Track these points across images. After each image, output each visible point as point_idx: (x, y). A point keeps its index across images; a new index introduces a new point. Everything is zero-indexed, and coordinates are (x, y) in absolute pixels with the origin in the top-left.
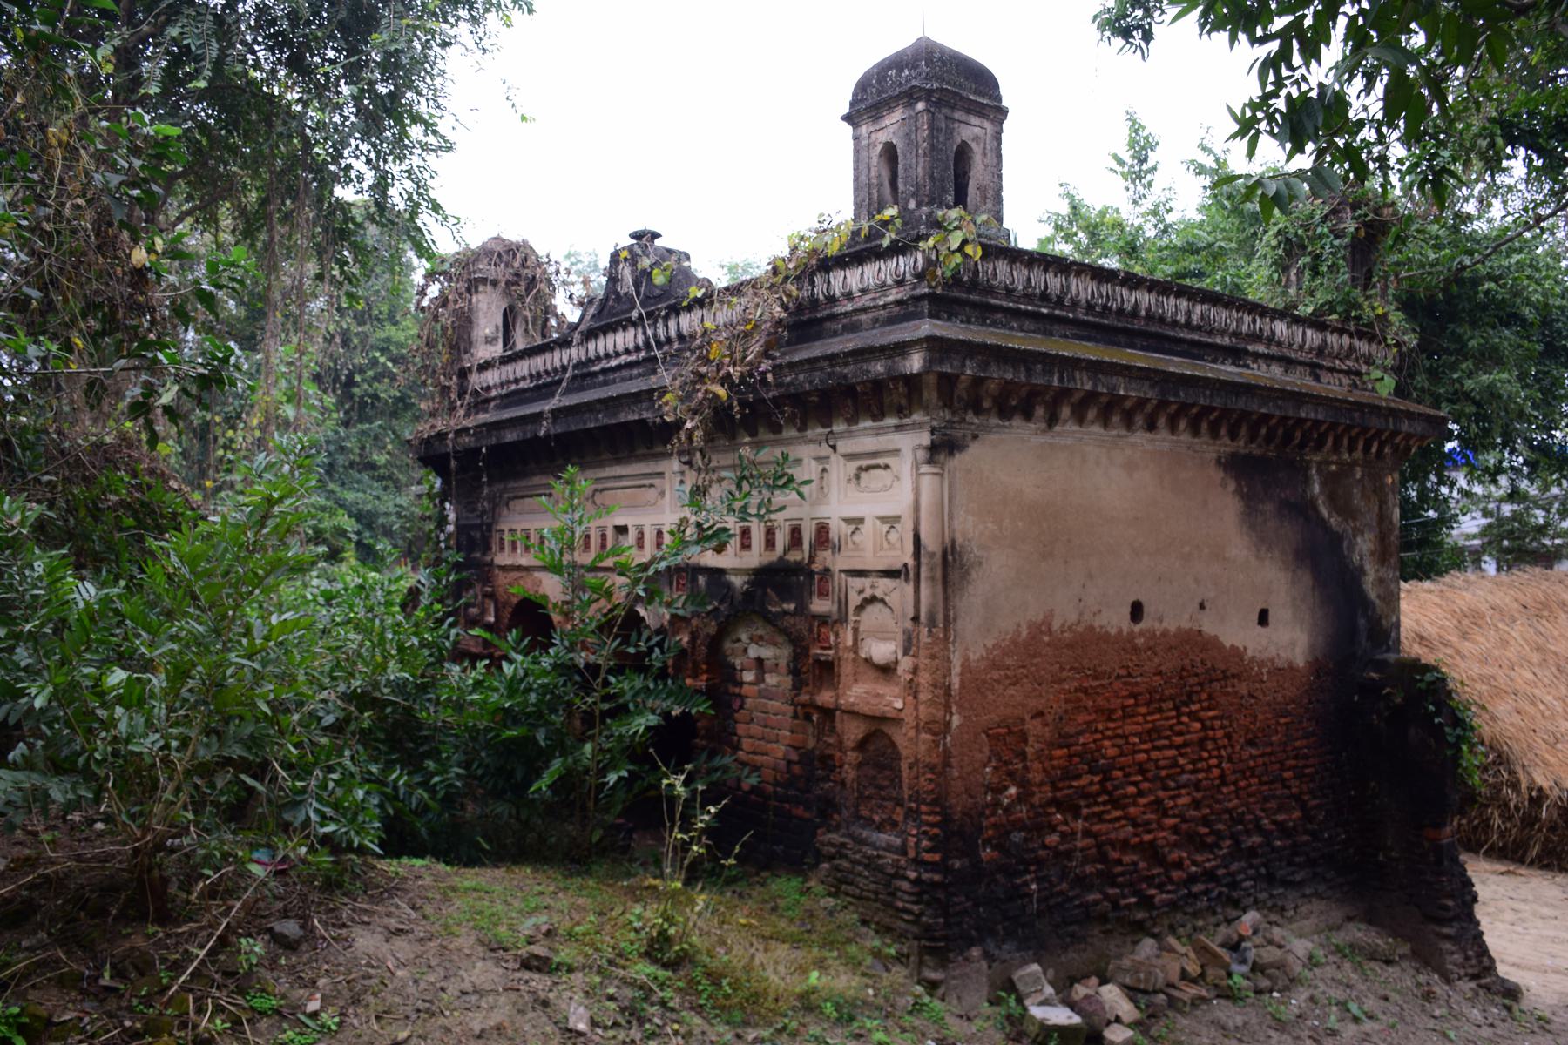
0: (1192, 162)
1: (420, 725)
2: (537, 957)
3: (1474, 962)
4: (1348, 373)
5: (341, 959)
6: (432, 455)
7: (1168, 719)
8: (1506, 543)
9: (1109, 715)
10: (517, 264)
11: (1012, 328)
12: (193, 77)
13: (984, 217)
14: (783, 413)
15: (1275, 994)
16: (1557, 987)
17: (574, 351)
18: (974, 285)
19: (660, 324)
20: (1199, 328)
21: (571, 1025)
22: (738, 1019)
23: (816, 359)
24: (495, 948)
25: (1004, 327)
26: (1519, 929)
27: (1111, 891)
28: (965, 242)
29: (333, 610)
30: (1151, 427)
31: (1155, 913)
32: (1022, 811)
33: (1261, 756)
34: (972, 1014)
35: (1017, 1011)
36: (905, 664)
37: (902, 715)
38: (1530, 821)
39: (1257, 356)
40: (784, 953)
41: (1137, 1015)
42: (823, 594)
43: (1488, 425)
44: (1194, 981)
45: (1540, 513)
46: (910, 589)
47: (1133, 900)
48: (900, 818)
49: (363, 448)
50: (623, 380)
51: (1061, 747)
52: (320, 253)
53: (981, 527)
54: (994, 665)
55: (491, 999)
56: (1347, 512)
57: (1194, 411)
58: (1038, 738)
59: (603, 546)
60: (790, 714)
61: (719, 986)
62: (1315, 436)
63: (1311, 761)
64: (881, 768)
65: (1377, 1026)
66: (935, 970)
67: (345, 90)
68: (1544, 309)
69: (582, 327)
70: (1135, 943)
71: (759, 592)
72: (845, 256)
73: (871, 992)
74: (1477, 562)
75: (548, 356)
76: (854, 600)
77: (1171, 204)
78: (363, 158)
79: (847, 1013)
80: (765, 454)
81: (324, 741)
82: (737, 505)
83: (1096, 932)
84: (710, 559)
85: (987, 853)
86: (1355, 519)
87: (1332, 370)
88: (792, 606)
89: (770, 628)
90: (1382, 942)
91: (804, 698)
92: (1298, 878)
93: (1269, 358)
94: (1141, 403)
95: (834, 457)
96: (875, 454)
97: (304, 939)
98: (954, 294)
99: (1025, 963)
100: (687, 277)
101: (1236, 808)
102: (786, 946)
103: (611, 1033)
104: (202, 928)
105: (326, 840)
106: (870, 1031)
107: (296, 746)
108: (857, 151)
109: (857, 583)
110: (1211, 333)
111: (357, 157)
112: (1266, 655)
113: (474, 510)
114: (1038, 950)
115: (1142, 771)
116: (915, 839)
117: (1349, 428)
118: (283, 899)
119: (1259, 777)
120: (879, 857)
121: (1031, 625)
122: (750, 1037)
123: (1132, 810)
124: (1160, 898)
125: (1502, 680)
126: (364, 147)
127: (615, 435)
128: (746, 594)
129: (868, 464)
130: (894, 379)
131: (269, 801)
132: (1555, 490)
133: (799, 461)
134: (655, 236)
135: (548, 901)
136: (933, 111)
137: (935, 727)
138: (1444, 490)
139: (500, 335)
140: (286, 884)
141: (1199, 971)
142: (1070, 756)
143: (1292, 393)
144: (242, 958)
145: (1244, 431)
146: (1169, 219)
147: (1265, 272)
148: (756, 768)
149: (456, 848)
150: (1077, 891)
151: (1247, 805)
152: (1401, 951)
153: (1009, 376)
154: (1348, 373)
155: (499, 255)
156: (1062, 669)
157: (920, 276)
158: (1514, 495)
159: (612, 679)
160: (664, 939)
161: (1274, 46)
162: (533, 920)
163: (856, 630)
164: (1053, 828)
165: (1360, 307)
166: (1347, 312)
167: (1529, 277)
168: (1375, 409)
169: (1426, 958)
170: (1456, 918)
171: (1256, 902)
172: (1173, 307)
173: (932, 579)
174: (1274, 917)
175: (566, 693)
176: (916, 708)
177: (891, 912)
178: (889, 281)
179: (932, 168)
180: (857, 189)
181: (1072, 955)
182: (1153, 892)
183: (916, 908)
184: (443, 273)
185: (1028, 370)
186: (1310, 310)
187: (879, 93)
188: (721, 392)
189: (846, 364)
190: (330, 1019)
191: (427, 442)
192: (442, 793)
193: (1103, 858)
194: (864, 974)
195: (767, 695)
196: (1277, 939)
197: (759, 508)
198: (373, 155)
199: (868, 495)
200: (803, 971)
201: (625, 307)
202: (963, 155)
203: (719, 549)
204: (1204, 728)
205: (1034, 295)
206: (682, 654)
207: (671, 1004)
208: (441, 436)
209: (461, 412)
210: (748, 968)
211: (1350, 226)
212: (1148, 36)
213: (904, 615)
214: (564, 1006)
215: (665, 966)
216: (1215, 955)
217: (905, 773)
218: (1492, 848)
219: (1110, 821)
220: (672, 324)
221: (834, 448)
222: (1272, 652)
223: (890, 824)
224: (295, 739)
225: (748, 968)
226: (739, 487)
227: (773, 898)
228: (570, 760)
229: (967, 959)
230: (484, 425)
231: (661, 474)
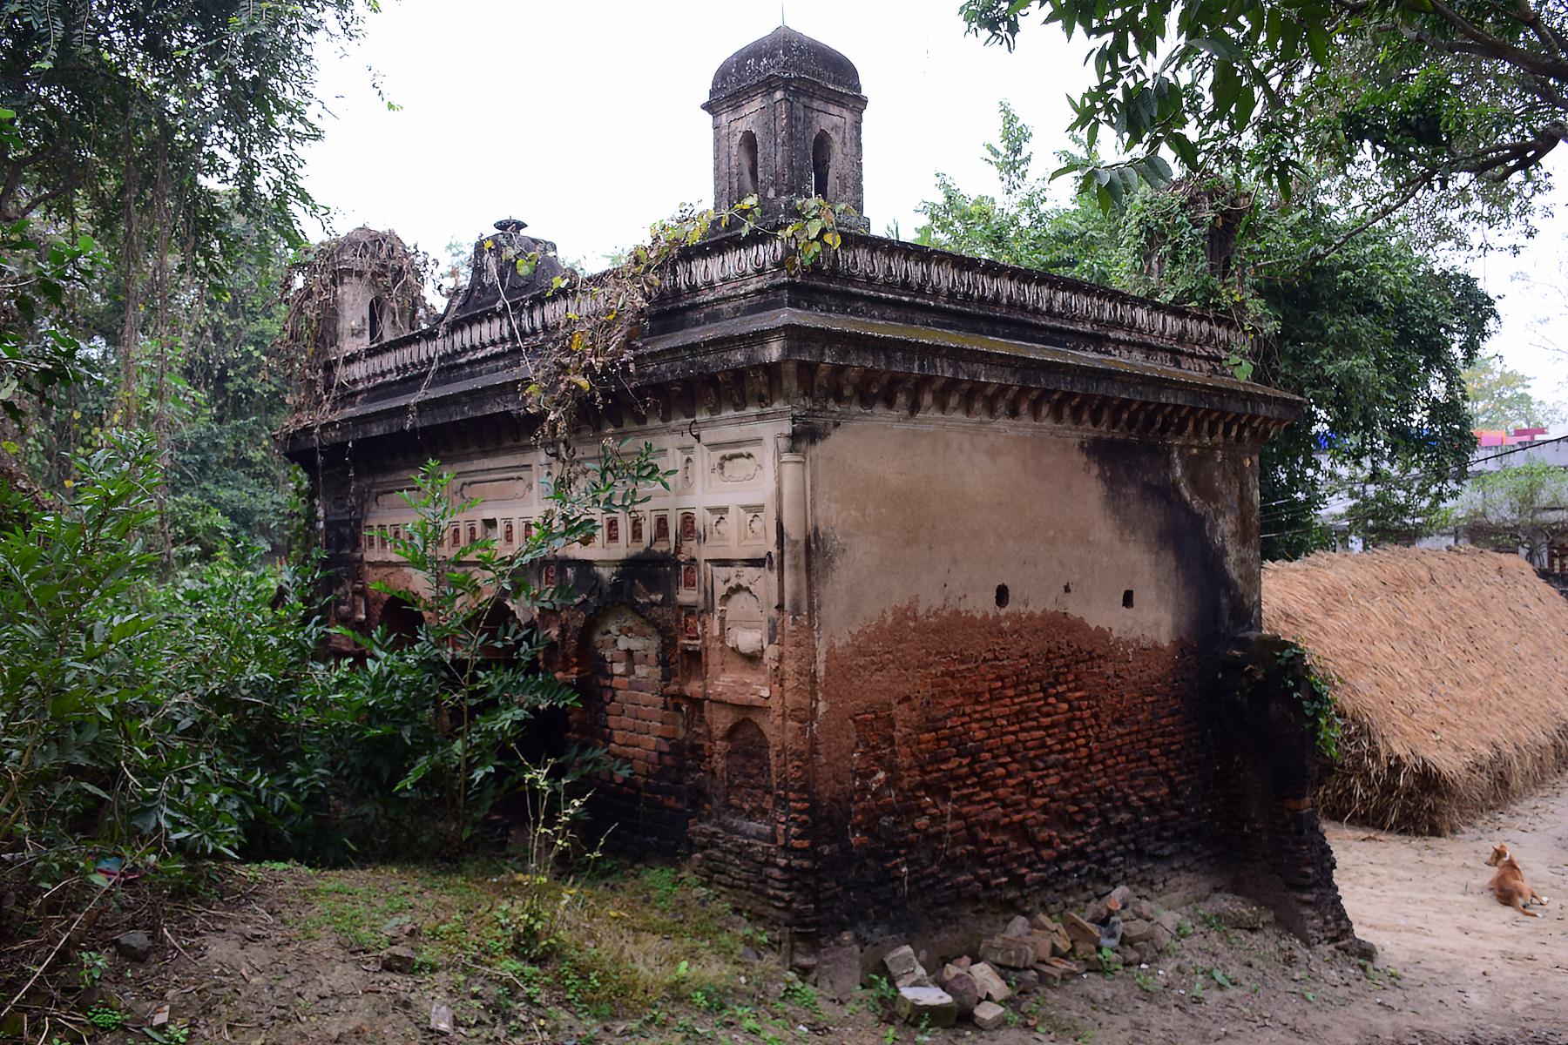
0: (1065, 153)
1: (284, 725)
2: (399, 958)
3: (1332, 925)
4: (1208, 358)
5: (192, 969)
6: (298, 450)
7: (1034, 700)
8: (1370, 522)
9: (976, 698)
10: (383, 255)
11: (873, 317)
12: (38, 57)
13: (843, 206)
14: (645, 403)
15: (1143, 966)
16: (1409, 945)
17: (440, 343)
18: (834, 273)
19: (525, 315)
20: (1061, 315)
21: (432, 1026)
22: (607, 1012)
23: (677, 349)
24: (355, 950)
25: (865, 315)
26: (1378, 892)
27: (981, 872)
28: (823, 231)
29: (195, 609)
30: (1014, 413)
31: (1026, 891)
32: (891, 795)
33: (1129, 734)
34: (844, 998)
36: (771, 652)
37: (769, 703)
38: (1389, 788)
41: (1007, 992)
42: (690, 584)
44: (1064, 957)
45: (1401, 494)
46: (774, 577)
47: (1004, 879)
48: (769, 806)
49: (238, 445)
50: (490, 372)
51: (928, 731)
52: (183, 243)
53: (844, 514)
54: (860, 652)
55: (350, 1003)
56: (1209, 494)
57: (1056, 397)
58: (906, 723)
59: (472, 540)
60: (661, 705)
61: (587, 979)
62: (1175, 420)
63: (1178, 737)
64: (749, 756)
65: (1240, 992)
66: (807, 956)
67: (206, 73)
68: (1396, 296)
69: (448, 319)
70: (1007, 922)
71: (627, 583)
72: (705, 245)
73: (743, 979)
74: (1345, 541)
75: (414, 348)
76: (721, 589)
77: (1045, 194)
78: (228, 146)
79: (718, 1001)
80: (629, 445)
81: (179, 745)
82: (603, 496)
83: (968, 912)
84: (577, 551)
85: (856, 838)
86: (1216, 502)
87: (1192, 356)
88: (660, 597)
89: (639, 620)
90: (1246, 911)
91: (673, 688)
92: (1166, 852)
93: (1130, 345)
94: (1003, 389)
95: (697, 447)
96: (737, 444)
97: (153, 949)
98: (813, 283)
99: (897, 945)
100: (552, 266)
101: (1105, 785)
102: (658, 937)
103: (474, 1032)
104: (41, 944)
106: (740, 1018)
107: (147, 752)
108: (717, 141)
109: (722, 572)
110: (1072, 320)
111: (220, 145)
113: (343, 506)
114: (909, 931)
115: (1011, 753)
116: (784, 825)
117: (1209, 412)
118: (132, 909)
119: (1127, 755)
120: (749, 845)
122: (618, 1031)
123: (1001, 791)
124: (1031, 876)
125: (1363, 655)
126: (228, 135)
127: (482, 429)
128: (615, 585)
129: (731, 453)
130: (754, 367)
131: (121, 809)
132: (1415, 471)
133: (663, 452)
134: (520, 226)
135: (413, 900)
136: (793, 100)
137: (802, 714)
138: (1310, 472)
139: (367, 327)
140: (137, 894)
141: (1070, 946)
142: (938, 740)
143: (1152, 378)
144: (84, 973)
146: (1043, 208)
147: (1130, 260)
148: (628, 760)
149: (321, 849)
150: (948, 873)
151: (1115, 782)
152: (1264, 919)
153: (869, 364)
154: (1208, 358)
155: (365, 246)
156: (928, 654)
157: (779, 265)
158: (1375, 477)
159: (481, 674)
160: (530, 934)
161: (1109, 37)
162: (396, 920)
163: (722, 619)
164: (922, 812)
165: (1219, 294)
166: (1206, 299)
167: (1383, 267)
168: (1233, 393)
169: (1288, 924)
170: (1316, 884)
171: (1125, 877)
172: (1033, 294)
173: (796, 567)
174: (1143, 891)
175: (431, 690)
176: (782, 696)
177: (762, 899)
178: (750, 271)
179: (791, 157)
181: (944, 935)
182: (1024, 871)
183: (786, 895)
184: (308, 264)
185: (888, 358)
186: (1171, 297)
187: (739, 81)
188: (584, 383)
189: (707, 353)
190: (178, 1031)
191: (293, 437)
192: (306, 794)
193: (973, 839)
194: (735, 963)
195: (637, 686)
196: (1145, 912)
197: (624, 500)
198: (237, 143)
199: (732, 484)
200: (674, 961)
201: (490, 298)
203: (585, 542)
204: (1071, 709)
205: (894, 283)
206: (552, 646)
207: (537, 1000)
208: (307, 431)
209: (328, 406)
210: (617, 961)
211: (1208, 216)
212: (1014, 28)
213: (769, 604)
214: (426, 1006)
215: (532, 962)
216: (1085, 931)
218: (1354, 816)
219: (980, 802)
220: (537, 314)
221: (698, 437)
222: (1137, 632)
223: (759, 812)
224: (146, 745)
225: (617, 961)
226: (604, 479)
227: (646, 890)
228: (437, 758)
229: (838, 944)
230: (350, 419)
231: (529, 466)
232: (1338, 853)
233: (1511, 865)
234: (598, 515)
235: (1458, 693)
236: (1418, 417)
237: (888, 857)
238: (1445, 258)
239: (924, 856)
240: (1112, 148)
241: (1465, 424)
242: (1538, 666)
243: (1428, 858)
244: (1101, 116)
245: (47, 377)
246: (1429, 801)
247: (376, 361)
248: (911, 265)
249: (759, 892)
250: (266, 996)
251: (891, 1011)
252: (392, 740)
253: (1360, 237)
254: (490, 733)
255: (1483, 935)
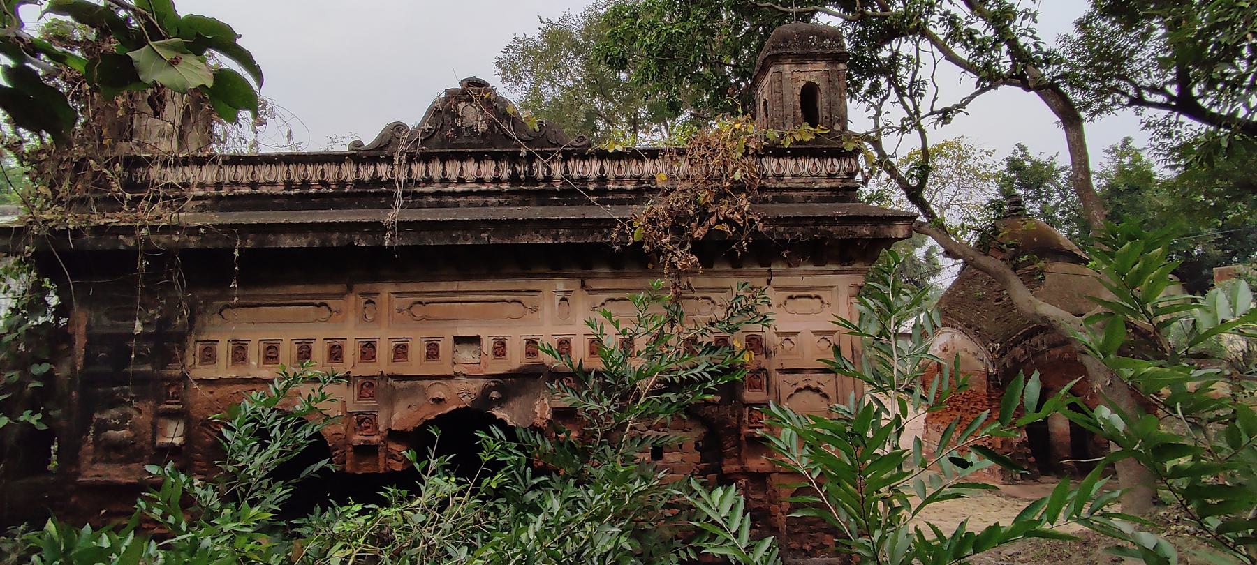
109: (790, 377)
178: (823, 173)
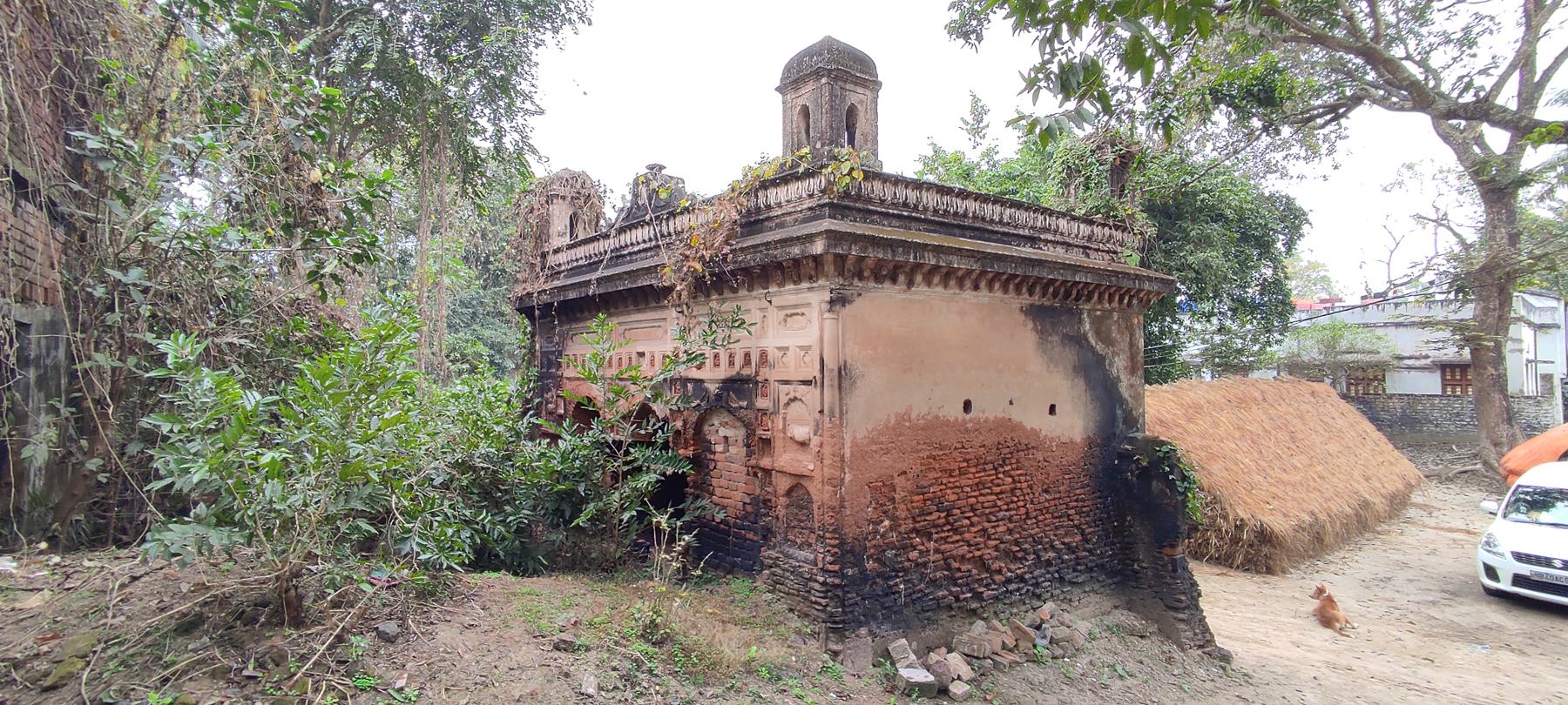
1: (503, 482)
5: (426, 648)
6: (525, 309)
18: (859, 197)
28: (852, 169)
30: (976, 287)
35: (891, 672)
36: (815, 441)
38: (1236, 540)
39: (1047, 241)
40: (737, 629)
41: (972, 675)
42: (765, 395)
43: (1203, 284)
44: (1011, 650)
54: (873, 442)
56: (1109, 342)
62: (1086, 293)
64: (801, 508)
68: (1240, 211)
74: (1198, 371)
76: (784, 399)
80: (727, 306)
82: (710, 339)
84: (695, 374)
85: (870, 565)
87: (1097, 250)
91: (753, 462)
96: (795, 306)
98: (845, 204)
100: (679, 193)
103: (611, 695)
105: (425, 565)
112: (1055, 434)
114: (904, 626)
115: (973, 510)
121: (897, 415)
127: (638, 297)
135: (578, 600)
136: (833, 84)
138: (1175, 327)
145: (1038, 289)
146: (996, 158)
149: (522, 563)
157: (823, 192)
158: (1221, 330)
160: (653, 625)
169: (1167, 634)
174: (1065, 606)
180: (785, 136)
181: (928, 632)
183: (823, 601)
188: (699, 267)
191: (521, 299)
193: (948, 567)
199: (790, 331)
200: (748, 645)
202: (852, 112)
208: (530, 295)
210: (710, 645)
211: (1110, 157)
212: (980, 38)
216: (1025, 633)
217: (816, 511)
220: (671, 223)
222: (1058, 432)
225: (710, 645)
232: (1202, 587)
233: (1330, 599)
234: (708, 351)
235: (1285, 477)
236: (1252, 291)
237: (890, 578)
238: (1272, 185)
239: (915, 577)
240: (1049, 104)
241: (1287, 295)
242: (1342, 459)
243: (1266, 590)
244: (1042, 84)
245: (358, 258)
246: (1265, 550)
247: (572, 251)
248: (909, 191)
249: (806, 599)
250: (474, 668)
251: (892, 684)
252: (572, 493)
253: (1213, 171)
254: (636, 489)
255: (1311, 649)
